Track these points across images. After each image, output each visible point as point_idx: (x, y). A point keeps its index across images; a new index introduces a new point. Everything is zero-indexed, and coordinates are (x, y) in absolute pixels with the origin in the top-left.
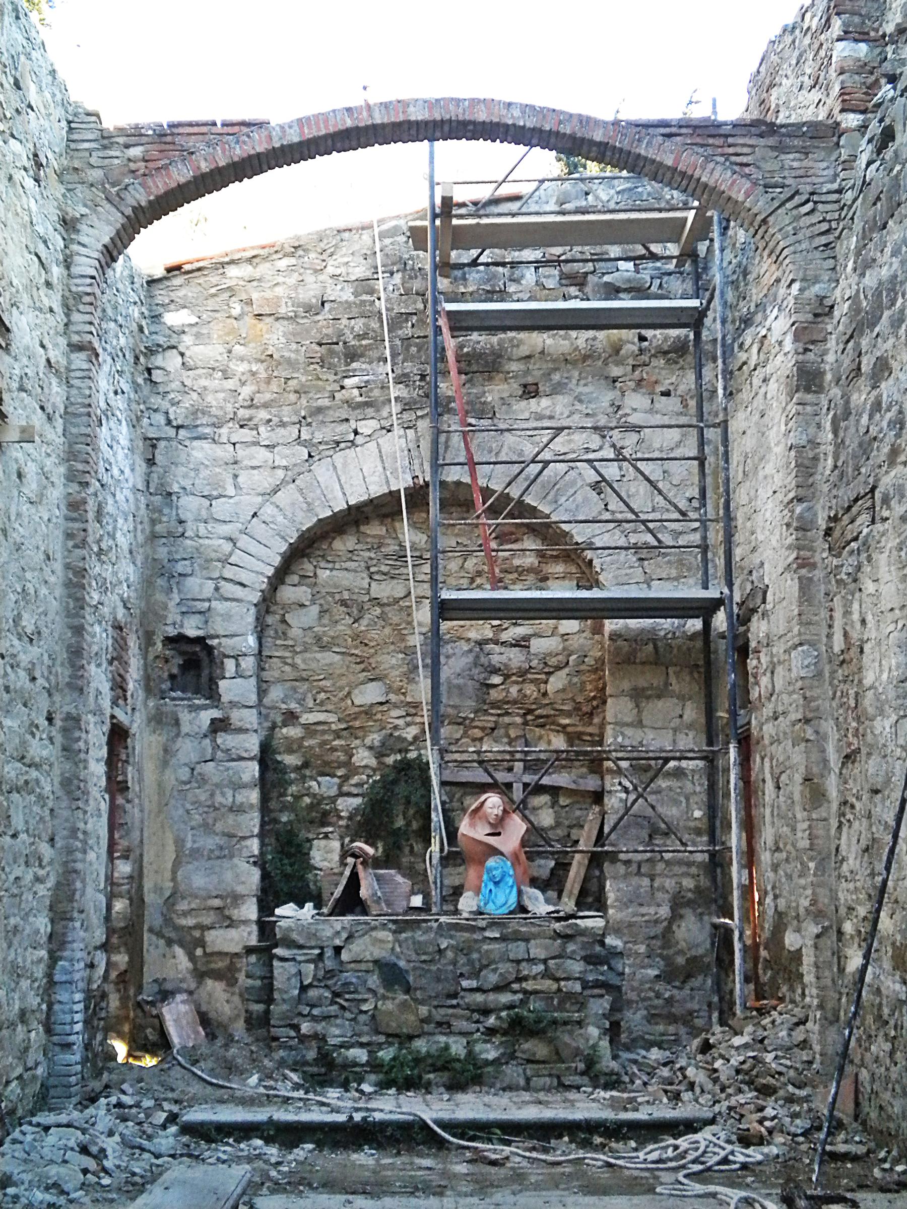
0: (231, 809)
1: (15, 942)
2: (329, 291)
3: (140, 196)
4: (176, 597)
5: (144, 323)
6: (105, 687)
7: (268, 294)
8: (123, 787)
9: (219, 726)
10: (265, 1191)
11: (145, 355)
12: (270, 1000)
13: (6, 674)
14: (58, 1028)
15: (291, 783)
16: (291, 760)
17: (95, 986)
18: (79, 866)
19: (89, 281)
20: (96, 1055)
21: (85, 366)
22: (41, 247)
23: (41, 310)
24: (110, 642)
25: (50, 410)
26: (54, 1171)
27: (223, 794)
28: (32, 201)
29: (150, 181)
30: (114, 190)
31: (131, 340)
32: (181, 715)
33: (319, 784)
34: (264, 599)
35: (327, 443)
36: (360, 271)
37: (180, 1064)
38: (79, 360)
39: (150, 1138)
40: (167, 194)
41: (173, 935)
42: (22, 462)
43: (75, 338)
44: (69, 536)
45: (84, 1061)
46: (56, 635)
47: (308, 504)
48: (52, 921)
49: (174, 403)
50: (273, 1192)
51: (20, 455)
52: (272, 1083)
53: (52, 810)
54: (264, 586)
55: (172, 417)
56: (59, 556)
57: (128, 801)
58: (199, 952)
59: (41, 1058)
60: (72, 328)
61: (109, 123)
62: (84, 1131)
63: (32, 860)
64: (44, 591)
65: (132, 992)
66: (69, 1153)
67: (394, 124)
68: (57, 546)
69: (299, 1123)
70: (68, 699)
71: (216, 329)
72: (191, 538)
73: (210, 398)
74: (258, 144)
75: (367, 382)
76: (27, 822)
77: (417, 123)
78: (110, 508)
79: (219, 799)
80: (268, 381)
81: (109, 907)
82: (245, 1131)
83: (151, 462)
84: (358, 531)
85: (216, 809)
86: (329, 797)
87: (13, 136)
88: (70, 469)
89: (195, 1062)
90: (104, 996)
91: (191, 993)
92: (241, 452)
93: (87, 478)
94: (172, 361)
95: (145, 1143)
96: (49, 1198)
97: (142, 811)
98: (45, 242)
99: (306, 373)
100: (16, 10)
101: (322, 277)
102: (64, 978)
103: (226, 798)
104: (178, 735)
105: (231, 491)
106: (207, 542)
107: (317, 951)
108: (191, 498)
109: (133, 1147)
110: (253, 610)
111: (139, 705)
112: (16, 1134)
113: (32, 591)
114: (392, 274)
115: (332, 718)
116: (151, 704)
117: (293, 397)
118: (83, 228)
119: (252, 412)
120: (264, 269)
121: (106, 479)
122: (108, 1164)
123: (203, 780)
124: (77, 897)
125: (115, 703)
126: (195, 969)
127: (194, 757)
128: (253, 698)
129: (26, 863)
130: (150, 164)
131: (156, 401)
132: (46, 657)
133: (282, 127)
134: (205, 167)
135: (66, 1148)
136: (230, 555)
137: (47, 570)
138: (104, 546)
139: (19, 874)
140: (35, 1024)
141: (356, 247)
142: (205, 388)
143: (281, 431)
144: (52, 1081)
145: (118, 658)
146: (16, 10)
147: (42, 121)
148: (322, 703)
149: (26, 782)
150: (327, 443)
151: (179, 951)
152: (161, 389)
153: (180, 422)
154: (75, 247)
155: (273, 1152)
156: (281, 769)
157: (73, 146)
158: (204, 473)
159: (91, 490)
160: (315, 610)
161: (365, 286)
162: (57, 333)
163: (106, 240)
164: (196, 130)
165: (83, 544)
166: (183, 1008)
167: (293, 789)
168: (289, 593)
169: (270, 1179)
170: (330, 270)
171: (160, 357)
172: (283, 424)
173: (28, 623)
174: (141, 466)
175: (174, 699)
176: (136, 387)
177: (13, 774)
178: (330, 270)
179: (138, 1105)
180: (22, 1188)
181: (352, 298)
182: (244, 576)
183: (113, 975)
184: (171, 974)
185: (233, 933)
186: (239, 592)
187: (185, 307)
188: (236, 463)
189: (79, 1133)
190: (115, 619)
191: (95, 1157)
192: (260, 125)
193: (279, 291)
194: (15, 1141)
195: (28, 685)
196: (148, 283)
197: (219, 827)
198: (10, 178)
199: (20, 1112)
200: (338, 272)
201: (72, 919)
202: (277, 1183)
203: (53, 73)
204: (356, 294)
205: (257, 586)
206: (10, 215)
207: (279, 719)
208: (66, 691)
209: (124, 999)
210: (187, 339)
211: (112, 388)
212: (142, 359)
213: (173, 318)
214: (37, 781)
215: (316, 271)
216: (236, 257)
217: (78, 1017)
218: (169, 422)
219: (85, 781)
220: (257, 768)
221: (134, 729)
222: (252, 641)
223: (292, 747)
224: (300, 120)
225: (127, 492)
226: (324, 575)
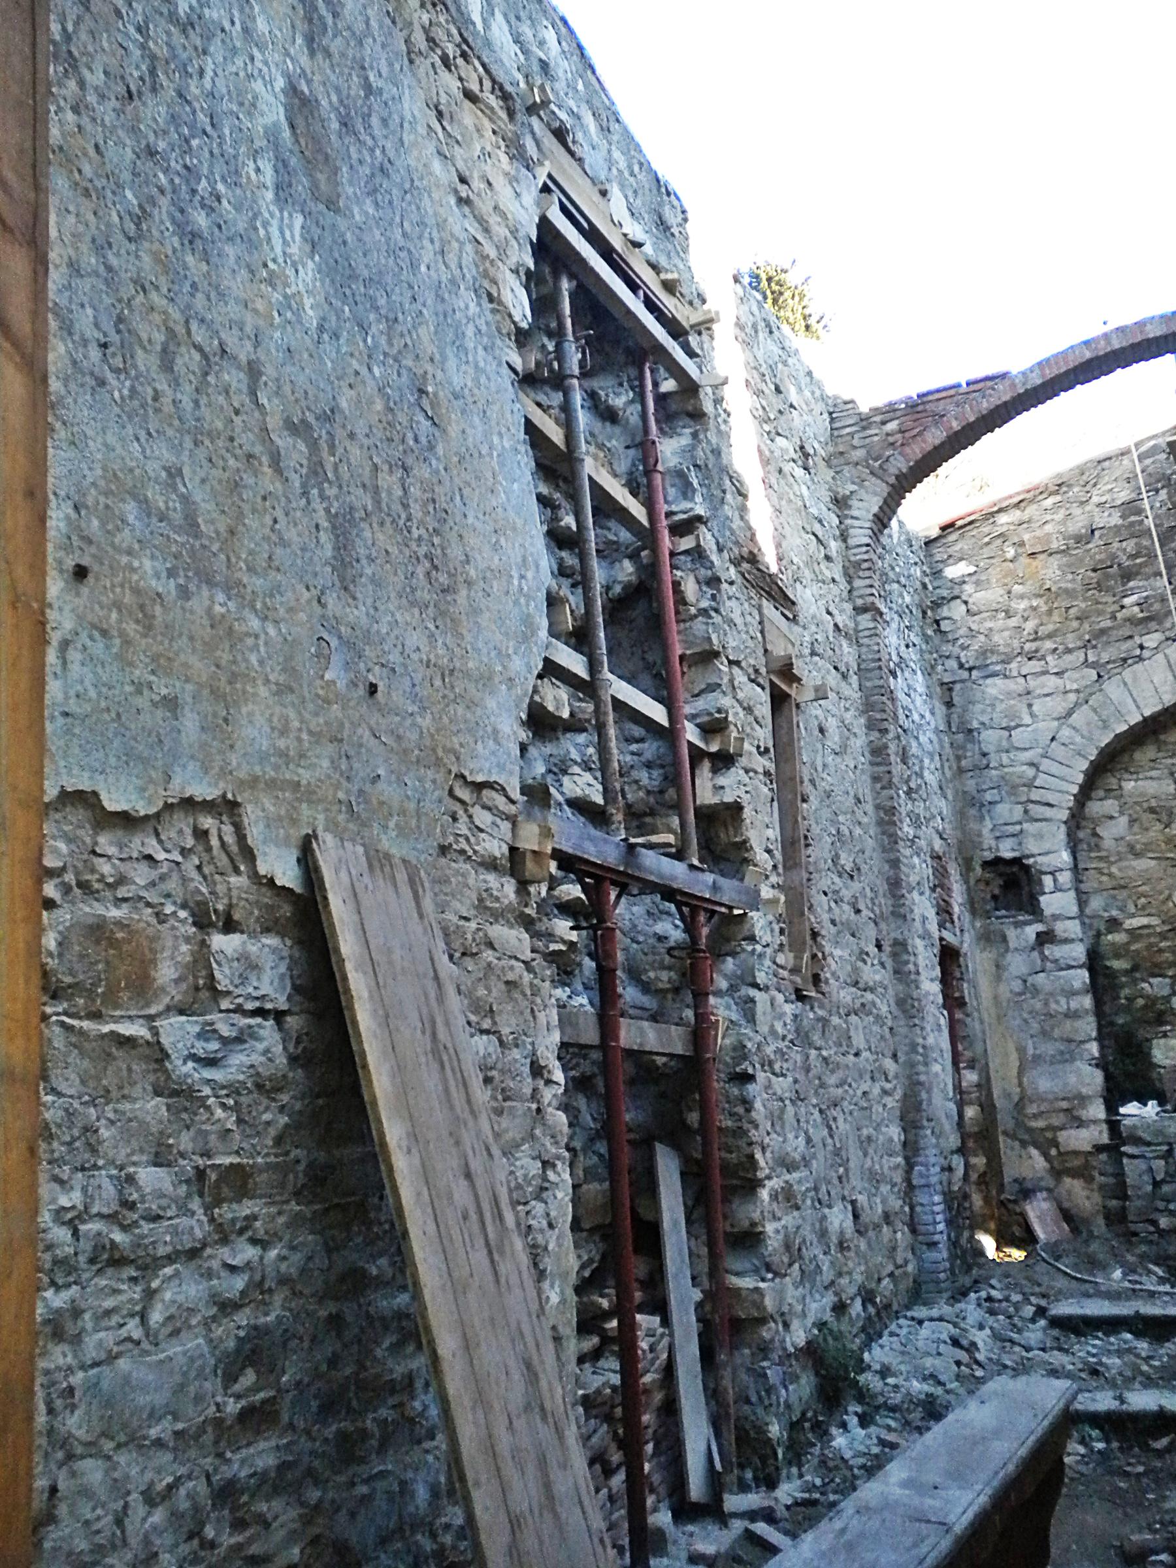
0: (1067, 1016)
1: (871, 1151)
2: (1097, 519)
3: (899, 464)
4: (988, 824)
5: (927, 580)
6: (931, 913)
7: (1038, 533)
8: (961, 1003)
9: (1045, 938)
10: (1137, 1385)
11: (932, 609)
12: (1125, 1197)
13: (830, 909)
14: (922, 1228)
15: (1122, 986)
16: (1117, 964)
17: (956, 1188)
18: (923, 1078)
19: (864, 549)
20: (964, 1252)
21: (871, 625)
22: (817, 528)
23: (824, 582)
24: (930, 871)
25: (843, 669)
26: (928, 1362)
27: (1057, 1002)
28: (804, 488)
29: (907, 450)
30: (877, 464)
31: (916, 597)
32: (1008, 933)
33: (1151, 985)
34: (1073, 816)
35: (1114, 662)
36: (1124, 495)
37: (1044, 1260)
38: (865, 620)
39: (1019, 1331)
40: (924, 457)
41: (1026, 1137)
42: (821, 717)
43: (859, 602)
44: (876, 779)
45: (953, 1257)
46: (876, 870)
47: (1104, 721)
48: (904, 1130)
49: (964, 648)
50: (1145, 1386)
51: (819, 712)
52: (1136, 1278)
53: (891, 1029)
54: (1071, 804)
55: (963, 660)
56: (869, 798)
57: (968, 1015)
58: (1053, 1152)
59: (910, 1256)
60: (855, 593)
61: (864, 408)
62: (955, 1325)
63: (877, 1075)
64: (858, 831)
65: (994, 1192)
66: (942, 1346)
67: (1133, 346)
68: (865, 789)
69: (1166, 1316)
70: (893, 926)
71: (994, 574)
72: (995, 768)
73: (996, 638)
74: (1003, 394)
75: (1147, 597)
76: (868, 1041)
77: (1156, 339)
78: (914, 749)
79: (1053, 1006)
80: (1050, 612)
81: (961, 1115)
82: (1111, 1325)
83: (949, 704)
84: (1157, 741)
85: (1052, 1016)
86: (1163, 997)
87: (779, 434)
88: (869, 719)
89: (1058, 1258)
90: (966, 1197)
91: (1049, 1190)
92: (1032, 683)
93: (885, 725)
94: (957, 610)
95: (1015, 1336)
96: (927, 1388)
97: (982, 1022)
98: (820, 521)
99: (1085, 599)
100: (768, 325)
101: (1088, 508)
102: (923, 1182)
103: (1062, 1005)
104: (1007, 950)
105: (1027, 720)
106: (1011, 770)
107: (1165, 1148)
108: (990, 732)
109: (1004, 1341)
110: (1063, 828)
111: (967, 926)
112: (893, 1327)
113: (847, 832)
114: (1157, 491)
115: (1154, 921)
116: (978, 924)
117: (1075, 624)
118: (854, 503)
119: (1037, 643)
120: (1031, 511)
121: (907, 724)
122: (980, 1357)
123: (1035, 991)
124: (924, 1106)
125: (941, 926)
126: (1052, 1168)
127: (1024, 970)
128: (1074, 910)
129: (872, 1078)
130: (907, 435)
131: (946, 649)
132: (868, 890)
133: (1024, 373)
134: (956, 426)
135: (939, 1341)
136: (1035, 778)
137: (859, 814)
138: (913, 785)
139: (867, 1089)
140: (900, 1226)
141: (1117, 473)
142: (991, 629)
143: (1068, 658)
144: (924, 1278)
145: (940, 884)
146: (768, 325)
147: (805, 417)
148: (1144, 908)
149: (863, 1005)
150: (1114, 662)
151: (1034, 1152)
152: (950, 637)
153: (971, 663)
154: (849, 522)
155: (1143, 1346)
156: (1111, 974)
157: (836, 433)
158: (1000, 707)
159: (891, 735)
160: (1124, 820)
161: (1131, 508)
162: (842, 600)
163: (875, 509)
164: (943, 394)
165: (890, 785)
166: (1045, 1205)
167: (1126, 992)
168: (1095, 808)
169: (1142, 1373)
170: (1095, 499)
171: (945, 608)
172: (1069, 651)
173: (846, 861)
174: (941, 710)
175: (998, 918)
176: (927, 639)
177: (849, 999)
178: (1095, 499)
179: (1007, 1299)
180: (902, 1377)
181: (1120, 522)
182: (1050, 797)
183: (974, 1176)
184: (1027, 1173)
185: (1084, 1133)
186: (1048, 812)
187: (961, 559)
188: (1028, 693)
189: (950, 1326)
190: (932, 850)
191: (967, 1350)
192: (1003, 376)
193: (1048, 528)
194: (892, 1334)
195: (853, 916)
196: (926, 544)
197: (1057, 1033)
198: (780, 471)
199: (895, 1307)
200: (1103, 499)
201: (922, 1127)
202: (1149, 1378)
203: (810, 374)
204: (1123, 517)
205: (1064, 805)
206: (784, 503)
207: (1103, 928)
208: (891, 919)
209: (987, 1200)
210: (969, 588)
211: (903, 643)
212: (929, 613)
213: (952, 572)
214: (874, 1004)
215: (1082, 503)
216: (1004, 505)
217: (939, 1218)
218: (961, 666)
219: (919, 1000)
220: (1087, 975)
221: (965, 948)
222: (1065, 856)
223: (1119, 952)
224: (1040, 364)
225: (929, 734)
226: (1129, 786)
